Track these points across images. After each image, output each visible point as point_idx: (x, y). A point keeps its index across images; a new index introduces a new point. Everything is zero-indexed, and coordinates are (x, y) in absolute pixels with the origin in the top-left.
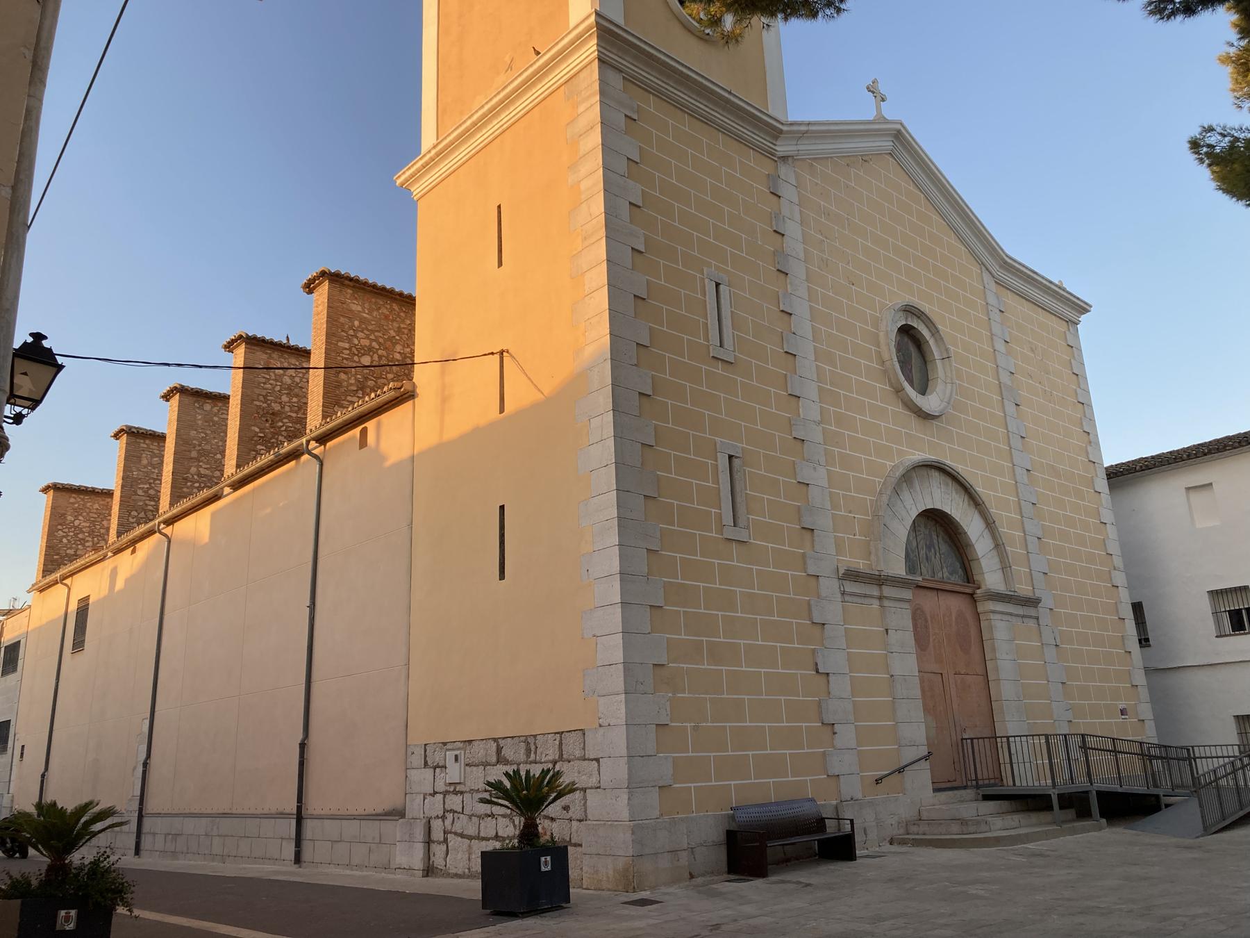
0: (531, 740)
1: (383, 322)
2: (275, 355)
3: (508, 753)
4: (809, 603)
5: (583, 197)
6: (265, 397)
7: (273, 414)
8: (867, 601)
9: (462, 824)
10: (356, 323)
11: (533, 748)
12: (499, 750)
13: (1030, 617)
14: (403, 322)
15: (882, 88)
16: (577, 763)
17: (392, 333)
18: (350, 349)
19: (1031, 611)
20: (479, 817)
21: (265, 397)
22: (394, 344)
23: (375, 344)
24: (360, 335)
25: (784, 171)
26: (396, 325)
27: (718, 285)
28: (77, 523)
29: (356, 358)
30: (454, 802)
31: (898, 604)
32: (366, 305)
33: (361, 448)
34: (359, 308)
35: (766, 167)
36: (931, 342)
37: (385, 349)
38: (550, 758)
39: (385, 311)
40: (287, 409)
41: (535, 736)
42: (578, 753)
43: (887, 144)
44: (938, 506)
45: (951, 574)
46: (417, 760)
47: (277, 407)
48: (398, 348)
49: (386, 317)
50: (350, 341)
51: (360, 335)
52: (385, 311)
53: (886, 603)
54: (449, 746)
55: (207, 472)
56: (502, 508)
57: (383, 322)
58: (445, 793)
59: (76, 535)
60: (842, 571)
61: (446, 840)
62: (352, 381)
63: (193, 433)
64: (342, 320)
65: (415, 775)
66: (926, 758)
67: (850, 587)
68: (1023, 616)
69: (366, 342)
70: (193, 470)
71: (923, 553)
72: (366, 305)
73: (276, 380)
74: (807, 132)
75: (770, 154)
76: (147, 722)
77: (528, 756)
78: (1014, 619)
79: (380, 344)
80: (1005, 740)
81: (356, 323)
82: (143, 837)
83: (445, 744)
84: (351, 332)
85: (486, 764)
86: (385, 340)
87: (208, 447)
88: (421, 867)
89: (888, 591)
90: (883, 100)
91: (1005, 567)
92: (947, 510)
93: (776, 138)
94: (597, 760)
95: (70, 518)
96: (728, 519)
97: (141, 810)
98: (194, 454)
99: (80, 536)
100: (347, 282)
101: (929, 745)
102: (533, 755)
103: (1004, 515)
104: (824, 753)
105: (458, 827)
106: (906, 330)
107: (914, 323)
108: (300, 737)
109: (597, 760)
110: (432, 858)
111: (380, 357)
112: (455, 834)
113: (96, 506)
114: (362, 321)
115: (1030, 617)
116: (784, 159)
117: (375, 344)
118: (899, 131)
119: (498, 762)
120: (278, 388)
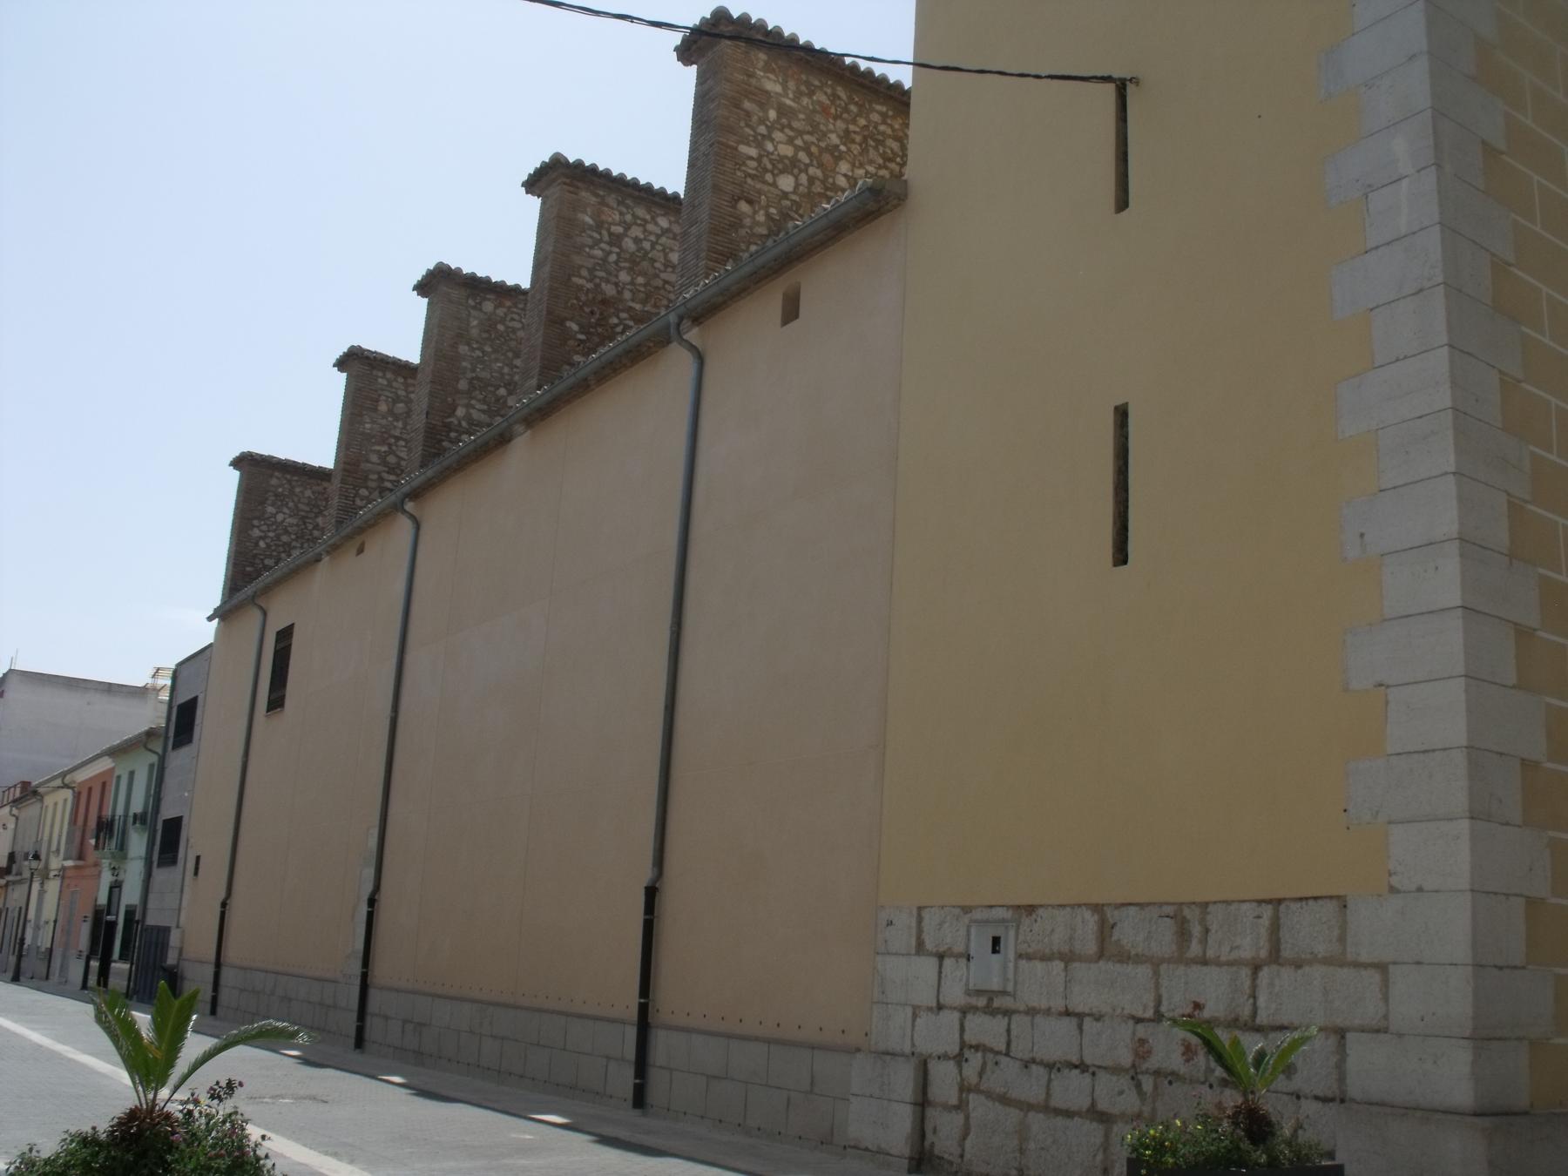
1: (818, 118)
2: (612, 200)
3: (1129, 932)
6: (591, 271)
9: (1007, 1076)
11: (1196, 930)
12: (1105, 929)
14: (854, 122)
17: (834, 139)
18: (759, 160)
20: (1050, 1066)
21: (591, 271)
22: (839, 158)
23: (802, 156)
24: (778, 135)
26: (840, 125)
28: (280, 517)
30: (986, 1030)
32: (791, 84)
33: (785, 322)
34: (778, 89)
37: (821, 165)
38: (1246, 953)
39: (823, 98)
40: (627, 295)
46: (901, 937)
47: (609, 290)
48: (844, 167)
49: (825, 110)
50: (760, 146)
51: (778, 135)
52: (823, 98)
54: (977, 915)
55: (483, 417)
56: (1122, 414)
57: (818, 118)
58: (964, 1011)
61: (961, 1106)
62: (761, 217)
64: (747, 105)
69: (787, 151)
70: (460, 412)
72: (791, 84)
73: (610, 244)
76: (375, 832)
79: (810, 154)
81: (772, 114)
82: (369, 1020)
83: (966, 910)
85: (1068, 958)
86: (821, 150)
87: (485, 375)
88: (907, 1152)
97: (364, 976)
99: (285, 538)
105: (994, 1081)
109: (1382, 967)
110: (930, 1137)
111: (811, 180)
112: (989, 1095)
113: (308, 493)
114: (783, 111)
117: (802, 156)
119: (1101, 955)
120: (613, 258)
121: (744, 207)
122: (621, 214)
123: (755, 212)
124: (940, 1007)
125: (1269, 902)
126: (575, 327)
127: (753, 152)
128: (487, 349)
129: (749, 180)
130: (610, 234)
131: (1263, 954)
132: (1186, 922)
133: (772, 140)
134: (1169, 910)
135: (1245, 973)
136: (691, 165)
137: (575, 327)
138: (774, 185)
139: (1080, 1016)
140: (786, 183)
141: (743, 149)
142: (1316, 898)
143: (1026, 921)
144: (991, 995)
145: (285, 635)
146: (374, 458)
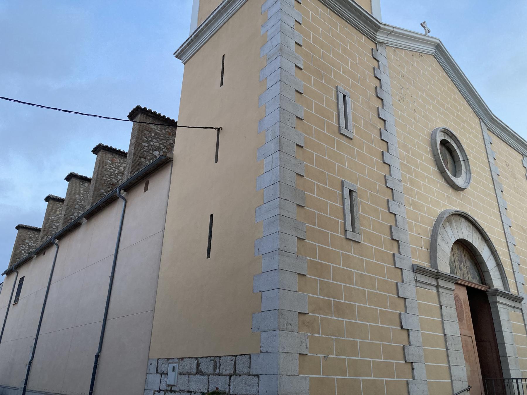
0: (217, 360)
2: (117, 156)
3: (203, 367)
4: (397, 283)
5: (268, 39)
6: (109, 176)
7: (112, 184)
8: (428, 287)
10: (153, 134)
11: (218, 365)
12: (198, 365)
13: (518, 308)
15: (428, 26)
16: (244, 377)
18: (148, 147)
19: (518, 305)
21: (109, 176)
25: (380, 48)
27: (344, 96)
28: (30, 244)
29: (151, 152)
31: (447, 292)
35: (372, 46)
36: (458, 151)
38: (228, 372)
39: (169, 131)
41: (220, 357)
42: (246, 370)
43: (432, 50)
44: (466, 238)
45: (473, 278)
46: (153, 369)
47: (115, 181)
50: (149, 143)
51: (154, 140)
52: (169, 131)
53: (440, 290)
54: (170, 361)
59: (29, 249)
60: (415, 268)
63: (78, 196)
64: (146, 132)
65: (151, 377)
66: (467, 390)
67: (421, 278)
68: (514, 307)
69: (157, 144)
71: (457, 264)
73: (116, 168)
74: (392, 31)
75: (373, 39)
77: (215, 370)
78: (509, 308)
80: (515, 381)
81: (153, 134)
83: (168, 359)
84: (150, 139)
85: (189, 374)
89: (441, 283)
90: (429, 32)
91: (503, 277)
92: (470, 241)
93: (377, 31)
94: (258, 376)
95: (27, 241)
96: (349, 227)
98: (77, 206)
100: (150, 114)
101: (469, 381)
102: (218, 370)
103: (501, 250)
104: (407, 381)
106: (444, 143)
107: (449, 140)
108: (97, 351)
109: (258, 376)
115: (518, 308)
116: (381, 43)
118: (438, 44)
120: (116, 172)
121: (143, 160)
122: (120, 160)
123: (146, 161)
124: (160, 390)
125: (234, 356)
126: (103, 191)
127: (147, 145)
128: (85, 196)
129: (145, 153)
130: (116, 166)
131: (232, 372)
132: (216, 361)
133: (153, 142)
134: (212, 358)
135: (228, 378)
136: (130, 148)
137: (103, 191)
138: (152, 154)
139: (191, 392)
140: (156, 153)
141: (143, 144)
142: (244, 355)
143: (181, 362)
144: (172, 386)
145: (22, 279)
146: (54, 227)
